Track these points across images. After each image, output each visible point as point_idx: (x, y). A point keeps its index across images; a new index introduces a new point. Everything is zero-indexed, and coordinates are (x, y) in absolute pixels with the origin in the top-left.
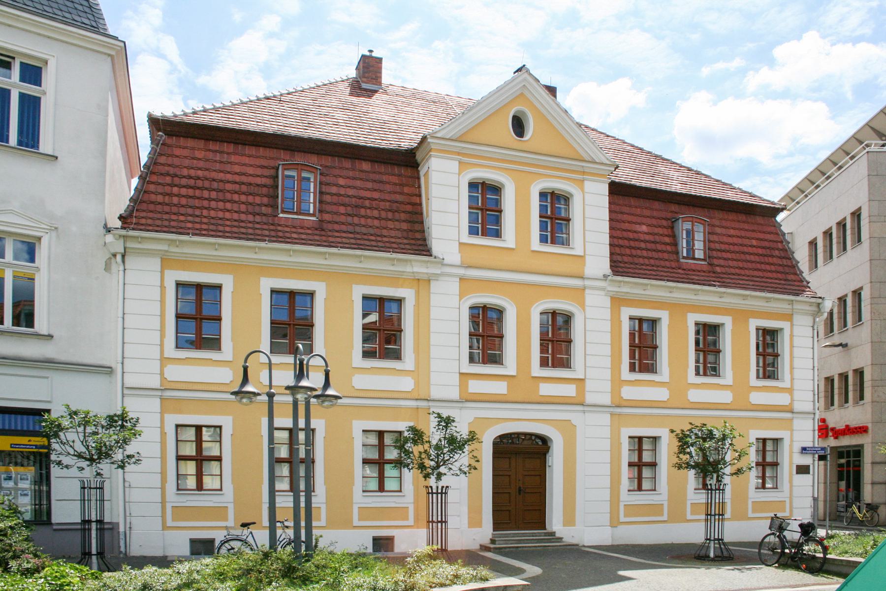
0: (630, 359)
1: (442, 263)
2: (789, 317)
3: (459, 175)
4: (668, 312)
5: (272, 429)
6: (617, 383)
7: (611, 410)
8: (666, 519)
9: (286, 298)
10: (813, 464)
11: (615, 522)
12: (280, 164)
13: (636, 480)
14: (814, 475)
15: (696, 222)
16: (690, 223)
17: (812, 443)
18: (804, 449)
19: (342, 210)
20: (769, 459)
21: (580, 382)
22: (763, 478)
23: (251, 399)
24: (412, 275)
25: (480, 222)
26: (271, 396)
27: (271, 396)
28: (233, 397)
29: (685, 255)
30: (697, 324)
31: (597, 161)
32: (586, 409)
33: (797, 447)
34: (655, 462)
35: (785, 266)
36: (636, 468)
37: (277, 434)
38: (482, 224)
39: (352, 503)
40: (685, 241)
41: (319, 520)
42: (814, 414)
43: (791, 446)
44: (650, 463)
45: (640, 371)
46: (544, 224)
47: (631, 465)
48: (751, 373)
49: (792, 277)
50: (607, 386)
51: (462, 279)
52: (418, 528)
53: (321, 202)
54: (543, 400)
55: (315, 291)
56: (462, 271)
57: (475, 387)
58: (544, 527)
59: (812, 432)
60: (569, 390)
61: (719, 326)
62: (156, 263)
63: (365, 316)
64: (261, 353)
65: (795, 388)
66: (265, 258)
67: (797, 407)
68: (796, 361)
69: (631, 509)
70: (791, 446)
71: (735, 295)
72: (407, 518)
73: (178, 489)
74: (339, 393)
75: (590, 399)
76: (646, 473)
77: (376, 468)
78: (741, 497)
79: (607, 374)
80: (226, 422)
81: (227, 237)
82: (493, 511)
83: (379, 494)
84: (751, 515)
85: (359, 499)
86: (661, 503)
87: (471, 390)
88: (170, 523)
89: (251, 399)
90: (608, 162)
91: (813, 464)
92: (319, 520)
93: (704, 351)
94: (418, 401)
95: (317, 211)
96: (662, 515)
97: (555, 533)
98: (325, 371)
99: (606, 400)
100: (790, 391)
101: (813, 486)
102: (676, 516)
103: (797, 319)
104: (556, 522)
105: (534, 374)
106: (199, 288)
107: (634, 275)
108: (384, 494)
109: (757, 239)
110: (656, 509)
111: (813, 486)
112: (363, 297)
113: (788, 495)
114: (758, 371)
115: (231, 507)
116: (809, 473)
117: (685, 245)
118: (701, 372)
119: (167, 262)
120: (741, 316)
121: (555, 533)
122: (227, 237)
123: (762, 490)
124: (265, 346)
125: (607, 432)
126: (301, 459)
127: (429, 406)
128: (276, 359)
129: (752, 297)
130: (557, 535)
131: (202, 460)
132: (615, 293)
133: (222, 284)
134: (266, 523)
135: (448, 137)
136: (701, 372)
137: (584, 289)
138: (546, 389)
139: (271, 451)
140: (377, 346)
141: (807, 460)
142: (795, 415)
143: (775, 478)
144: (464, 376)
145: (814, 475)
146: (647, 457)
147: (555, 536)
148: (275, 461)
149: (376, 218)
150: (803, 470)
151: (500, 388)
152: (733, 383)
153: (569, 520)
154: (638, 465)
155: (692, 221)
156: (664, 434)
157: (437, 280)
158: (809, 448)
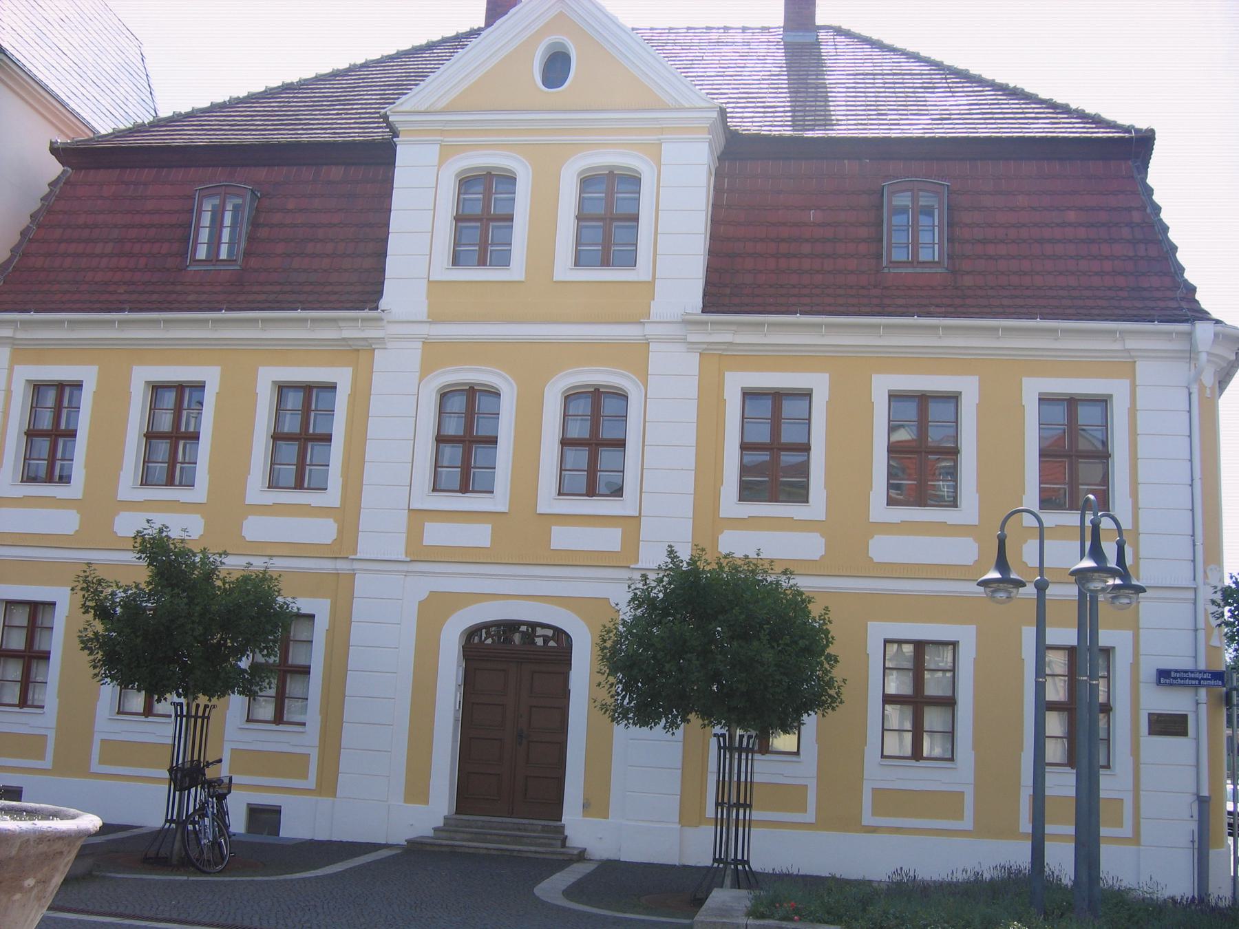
2: (1126, 367)
3: (440, 166)
5: (1042, 648)
9: (768, 403)
10: (1197, 712)
12: (883, 186)
14: (1197, 739)
15: (921, 190)
16: (909, 194)
17: (1192, 660)
18: (1165, 677)
21: (631, 524)
23: (1010, 593)
24: (1127, 355)
26: (1041, 587)
27: (1041, 587)
28: (982, 589)
31: (687, 106)
33: (1148, 671)
37: (1051, 656)
39: (223, 740)
42: (1195, 589)
43: (1135, 666)
48: (251, 479)
51: (427, 343)
52: (320, 795)
53: (951, 240)
55: (1111, 396)
56: (425, 330)
57: (436, 534)
59: (1191, 634)
63: (892, 429)
64: (1024, 513)
69: (888, 800)
70: (1135, 666)
72: (959, 815)
73: (883, 756)
74: (1022, 577)
77: (908, 711)
80: (966, 635)
81: (973, 313)
83: (274, 727)
85: (876, 775)
87: (427, 541)
89: (1010, 593)
90: (703, 104)
91: (1197, 712)
94: (338, 561)
95: (946, 256)
96: (42, 757)
98: (1117, 543)
101: (1197, 766)
103: (1144, 369)
106: (777, 397)
107: (253, 306)
108: (281, 727)
110: (948, 803)
111: (1197, 766)
112: (890, 396)
113: (1129, 784)
115: (812, 785)
122: (973, 313)
124: (1031, 499)
126: (1101, 704)
127: (354, 570)
128: (1052, 519)
131: (286, 672)
132: (705, 346)
133: (336, 383)
134: (1026, 826)
135: (423, 109)
137: (645, 343)
138: (563, 538)
139: (1040, 689)
140: (1066, 487)
144: (418, 516)
148: (1044, 706)
151: (479, 536)
152: (207, 501)
153: (595, 805)
155: (912, 190)
156: (64, 598)
157: (386, 348)
158: (1176, 671)
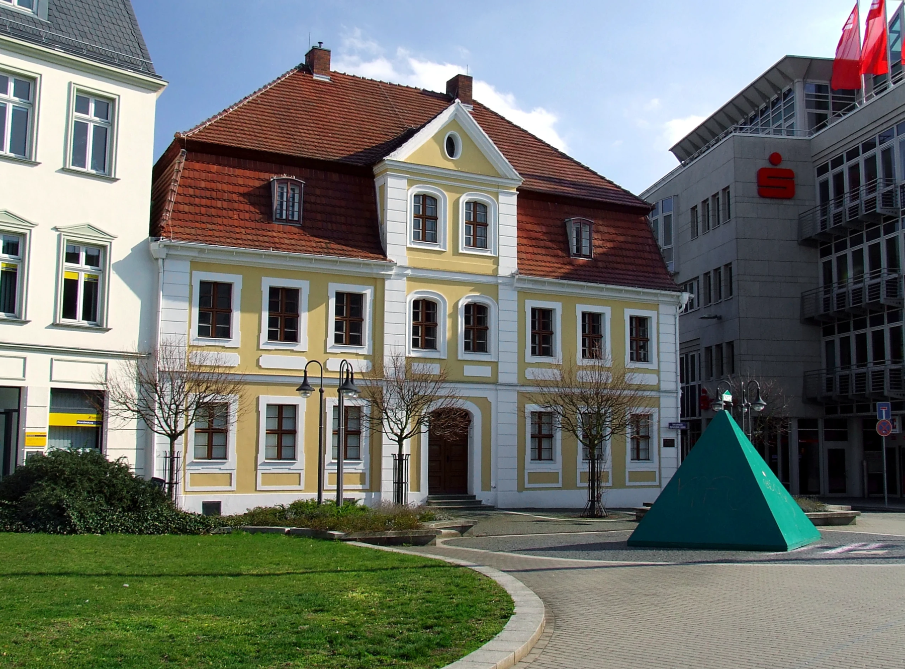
0: (583, 346)
1: (392, 264)
2: (655, 307)
4: (610, 308)
6: (523, 365)
7: (518, 388)
8: (611, 485)
10: (677, 438)
11: (521, 488)
13: (537, 450)
19: (319, 217)
20: (545, 431)
22: (540, 449)
25: (421, 228)
29: (575, 252)
30: (631, 318)
32: (499, 387)
34: (648, 436)
35: (655, 260)
36: (537, 440)
38: (422, 229)
40: (575, 240)
41: (607, 481)
44: (547, 435)
45: (540, 355)
46: (417, 221)
47: (533, 436)
49: (660, 270)
50: (515, 368)
54: (466, 380)
58: (466, 492)
60: (485, 372)
61: (647, 318)
62: (187, 265)
65: (662, 369)
66: (344, 269)
67: (663, 386)
68: (661, 345)
71: (612, 289)
75: (502, 379)
76: (545, 444)
78: (618, 465)
79: (515, 357)
82: (429, 476)
84: (628, 484)
86: (556, 471)
88: (657, 483)
92: (607, 481)
93: (636, 340)
97: (475, 496)
99: (514, 379)
100: (658, 372)
102: (569, 484)
104: (476, 487)
105: (460, 358)
109: (632, 236)
110: (553, 477)
114: (632, 354)
116: (674, 446)
117: (575, 243)
118: (635, 359)
119: (196, 265)
120: (252, 273)
121: (475, 496)
123: (637, 461)
125: (514, 407)
129: (607, 289)
130: (477, 499)
136: (635, 359)
138: (470, 371)
141: (671, 435)
142: (661, 394)
143: (647, 450)
145: (677, 448)
146: (286, 426)
147: (475, 499)
149: (344, 224)
150: (669, 443)
154: (538, 437)
